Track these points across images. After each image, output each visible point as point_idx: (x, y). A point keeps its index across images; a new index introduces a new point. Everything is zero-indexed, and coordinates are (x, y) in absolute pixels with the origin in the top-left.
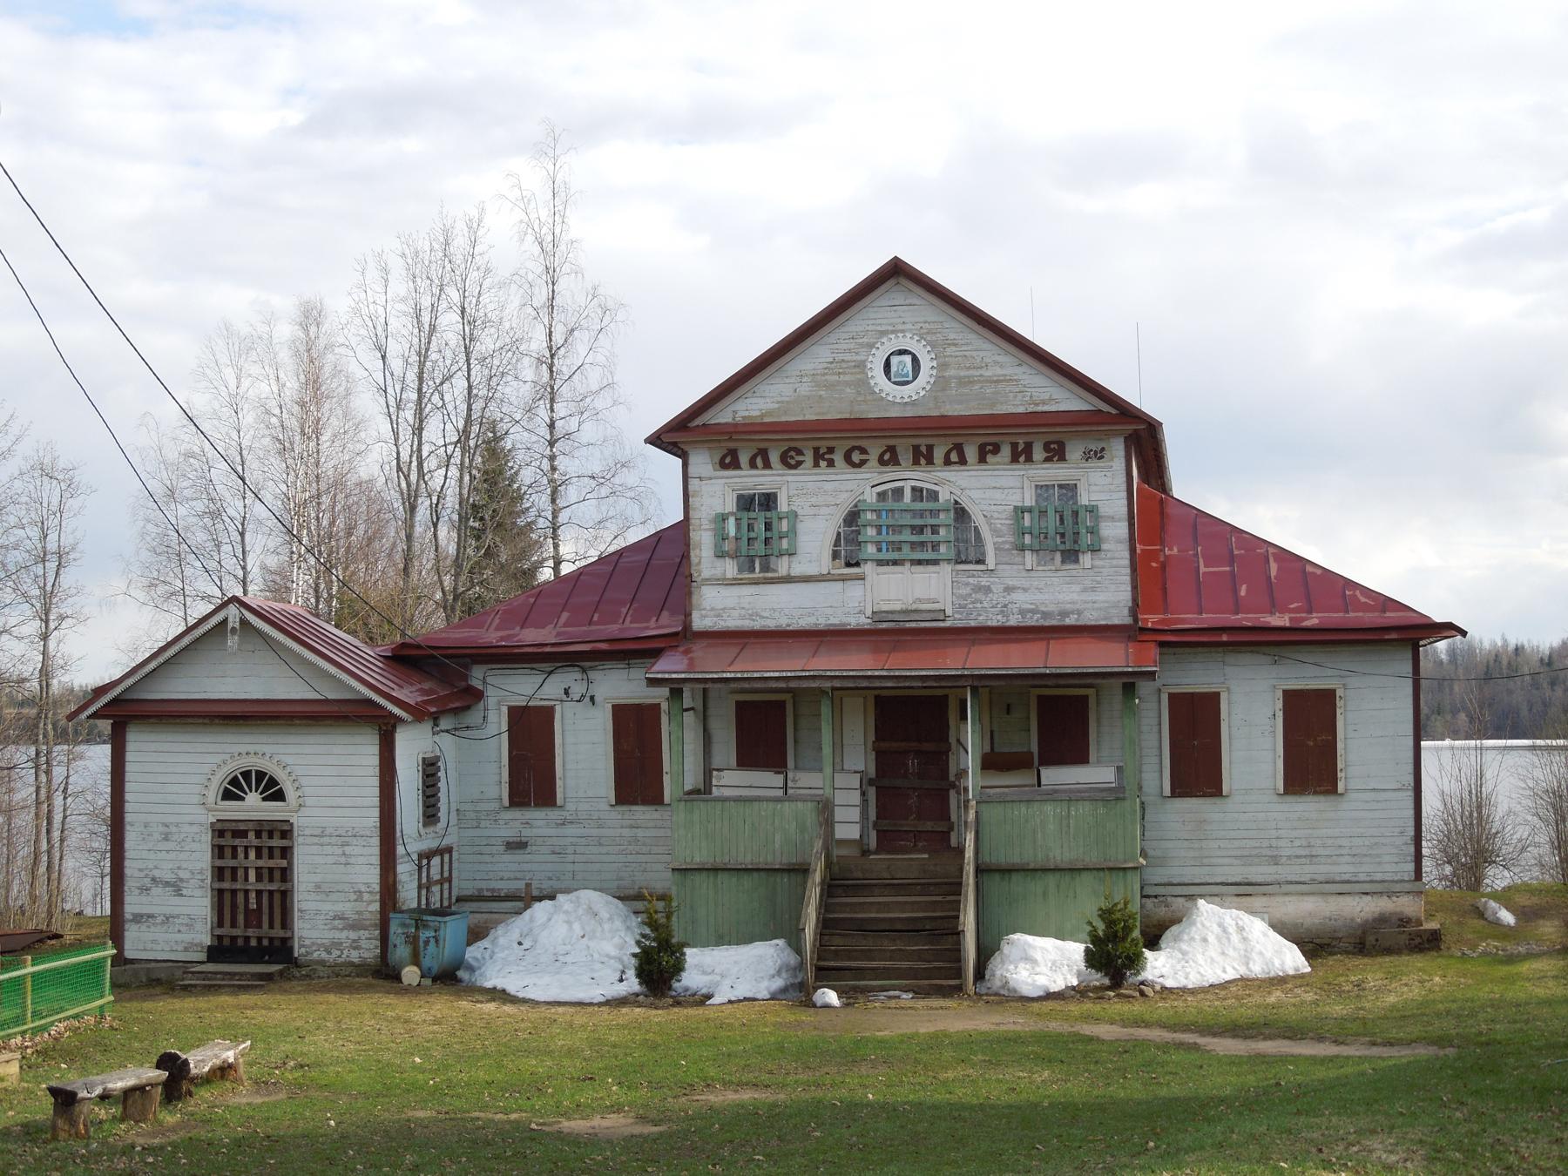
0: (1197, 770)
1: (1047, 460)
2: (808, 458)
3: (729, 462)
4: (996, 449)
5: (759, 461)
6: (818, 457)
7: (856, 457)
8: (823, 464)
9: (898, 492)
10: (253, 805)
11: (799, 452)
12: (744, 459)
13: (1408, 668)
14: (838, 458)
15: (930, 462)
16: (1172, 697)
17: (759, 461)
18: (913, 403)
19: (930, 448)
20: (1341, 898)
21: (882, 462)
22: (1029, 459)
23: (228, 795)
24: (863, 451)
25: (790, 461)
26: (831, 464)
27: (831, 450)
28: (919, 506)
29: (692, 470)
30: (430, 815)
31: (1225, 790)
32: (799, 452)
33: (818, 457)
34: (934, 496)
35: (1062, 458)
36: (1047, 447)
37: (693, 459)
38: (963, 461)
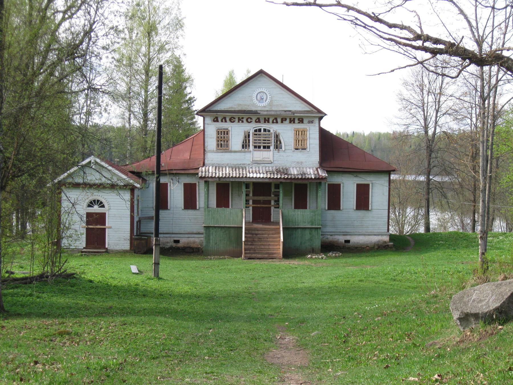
0: (334, 202)
1: (299, 123)
2: (237, 120)
3: (216, 120)
4: (286, 120)
5: (224, 120)
6: (239, 120)
7: (249, 120)
8: (240, 122)
9: (260, 130)
10: (96, 209)
11: (234, 118)
12: (220, 120)
13: (387, 179)
14: (245, 120)
15: (268, 122)
16: (329, 185)
17: (224, 120)
18: (265, 107)
19: (269, 119)
20: (369, 236)
21: (256, 122)
22: (294, 122)
23: (89, 206)
24: (251, 119)
25: (232, 120)
26: (243, 122)
27: (243, 118)
28: (265, 133)
29: (206, 122)
30: (491, 172)
31: (341, 208)
32: (234, 118)
33: (239, 120)
34: (269, 131)
35: (303, 122)
36: (299, 119)
37: (206, 119)
38: (277, 122)
